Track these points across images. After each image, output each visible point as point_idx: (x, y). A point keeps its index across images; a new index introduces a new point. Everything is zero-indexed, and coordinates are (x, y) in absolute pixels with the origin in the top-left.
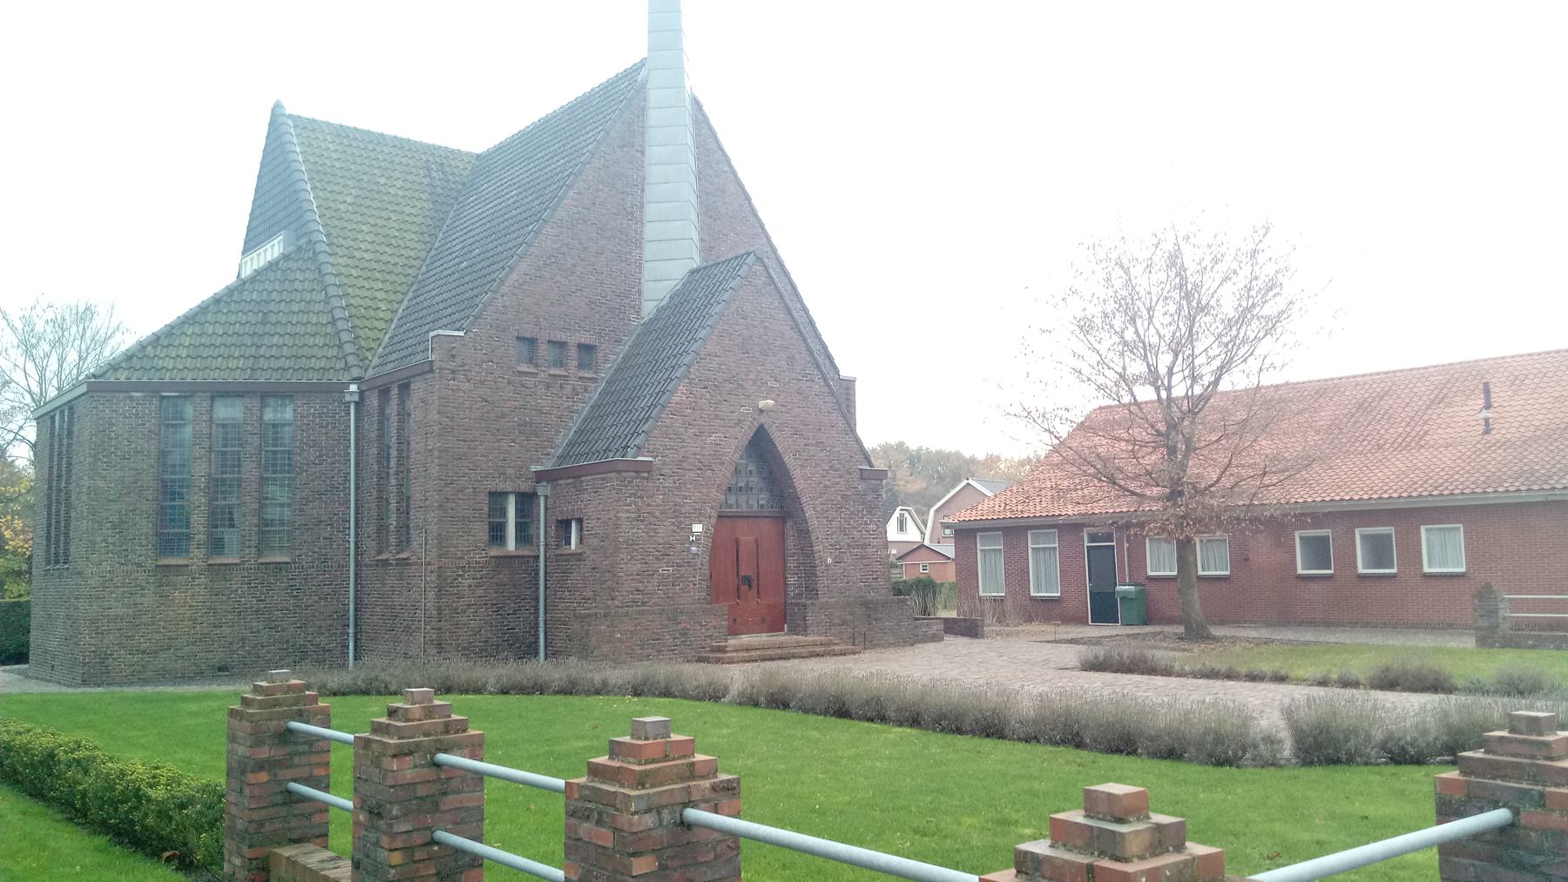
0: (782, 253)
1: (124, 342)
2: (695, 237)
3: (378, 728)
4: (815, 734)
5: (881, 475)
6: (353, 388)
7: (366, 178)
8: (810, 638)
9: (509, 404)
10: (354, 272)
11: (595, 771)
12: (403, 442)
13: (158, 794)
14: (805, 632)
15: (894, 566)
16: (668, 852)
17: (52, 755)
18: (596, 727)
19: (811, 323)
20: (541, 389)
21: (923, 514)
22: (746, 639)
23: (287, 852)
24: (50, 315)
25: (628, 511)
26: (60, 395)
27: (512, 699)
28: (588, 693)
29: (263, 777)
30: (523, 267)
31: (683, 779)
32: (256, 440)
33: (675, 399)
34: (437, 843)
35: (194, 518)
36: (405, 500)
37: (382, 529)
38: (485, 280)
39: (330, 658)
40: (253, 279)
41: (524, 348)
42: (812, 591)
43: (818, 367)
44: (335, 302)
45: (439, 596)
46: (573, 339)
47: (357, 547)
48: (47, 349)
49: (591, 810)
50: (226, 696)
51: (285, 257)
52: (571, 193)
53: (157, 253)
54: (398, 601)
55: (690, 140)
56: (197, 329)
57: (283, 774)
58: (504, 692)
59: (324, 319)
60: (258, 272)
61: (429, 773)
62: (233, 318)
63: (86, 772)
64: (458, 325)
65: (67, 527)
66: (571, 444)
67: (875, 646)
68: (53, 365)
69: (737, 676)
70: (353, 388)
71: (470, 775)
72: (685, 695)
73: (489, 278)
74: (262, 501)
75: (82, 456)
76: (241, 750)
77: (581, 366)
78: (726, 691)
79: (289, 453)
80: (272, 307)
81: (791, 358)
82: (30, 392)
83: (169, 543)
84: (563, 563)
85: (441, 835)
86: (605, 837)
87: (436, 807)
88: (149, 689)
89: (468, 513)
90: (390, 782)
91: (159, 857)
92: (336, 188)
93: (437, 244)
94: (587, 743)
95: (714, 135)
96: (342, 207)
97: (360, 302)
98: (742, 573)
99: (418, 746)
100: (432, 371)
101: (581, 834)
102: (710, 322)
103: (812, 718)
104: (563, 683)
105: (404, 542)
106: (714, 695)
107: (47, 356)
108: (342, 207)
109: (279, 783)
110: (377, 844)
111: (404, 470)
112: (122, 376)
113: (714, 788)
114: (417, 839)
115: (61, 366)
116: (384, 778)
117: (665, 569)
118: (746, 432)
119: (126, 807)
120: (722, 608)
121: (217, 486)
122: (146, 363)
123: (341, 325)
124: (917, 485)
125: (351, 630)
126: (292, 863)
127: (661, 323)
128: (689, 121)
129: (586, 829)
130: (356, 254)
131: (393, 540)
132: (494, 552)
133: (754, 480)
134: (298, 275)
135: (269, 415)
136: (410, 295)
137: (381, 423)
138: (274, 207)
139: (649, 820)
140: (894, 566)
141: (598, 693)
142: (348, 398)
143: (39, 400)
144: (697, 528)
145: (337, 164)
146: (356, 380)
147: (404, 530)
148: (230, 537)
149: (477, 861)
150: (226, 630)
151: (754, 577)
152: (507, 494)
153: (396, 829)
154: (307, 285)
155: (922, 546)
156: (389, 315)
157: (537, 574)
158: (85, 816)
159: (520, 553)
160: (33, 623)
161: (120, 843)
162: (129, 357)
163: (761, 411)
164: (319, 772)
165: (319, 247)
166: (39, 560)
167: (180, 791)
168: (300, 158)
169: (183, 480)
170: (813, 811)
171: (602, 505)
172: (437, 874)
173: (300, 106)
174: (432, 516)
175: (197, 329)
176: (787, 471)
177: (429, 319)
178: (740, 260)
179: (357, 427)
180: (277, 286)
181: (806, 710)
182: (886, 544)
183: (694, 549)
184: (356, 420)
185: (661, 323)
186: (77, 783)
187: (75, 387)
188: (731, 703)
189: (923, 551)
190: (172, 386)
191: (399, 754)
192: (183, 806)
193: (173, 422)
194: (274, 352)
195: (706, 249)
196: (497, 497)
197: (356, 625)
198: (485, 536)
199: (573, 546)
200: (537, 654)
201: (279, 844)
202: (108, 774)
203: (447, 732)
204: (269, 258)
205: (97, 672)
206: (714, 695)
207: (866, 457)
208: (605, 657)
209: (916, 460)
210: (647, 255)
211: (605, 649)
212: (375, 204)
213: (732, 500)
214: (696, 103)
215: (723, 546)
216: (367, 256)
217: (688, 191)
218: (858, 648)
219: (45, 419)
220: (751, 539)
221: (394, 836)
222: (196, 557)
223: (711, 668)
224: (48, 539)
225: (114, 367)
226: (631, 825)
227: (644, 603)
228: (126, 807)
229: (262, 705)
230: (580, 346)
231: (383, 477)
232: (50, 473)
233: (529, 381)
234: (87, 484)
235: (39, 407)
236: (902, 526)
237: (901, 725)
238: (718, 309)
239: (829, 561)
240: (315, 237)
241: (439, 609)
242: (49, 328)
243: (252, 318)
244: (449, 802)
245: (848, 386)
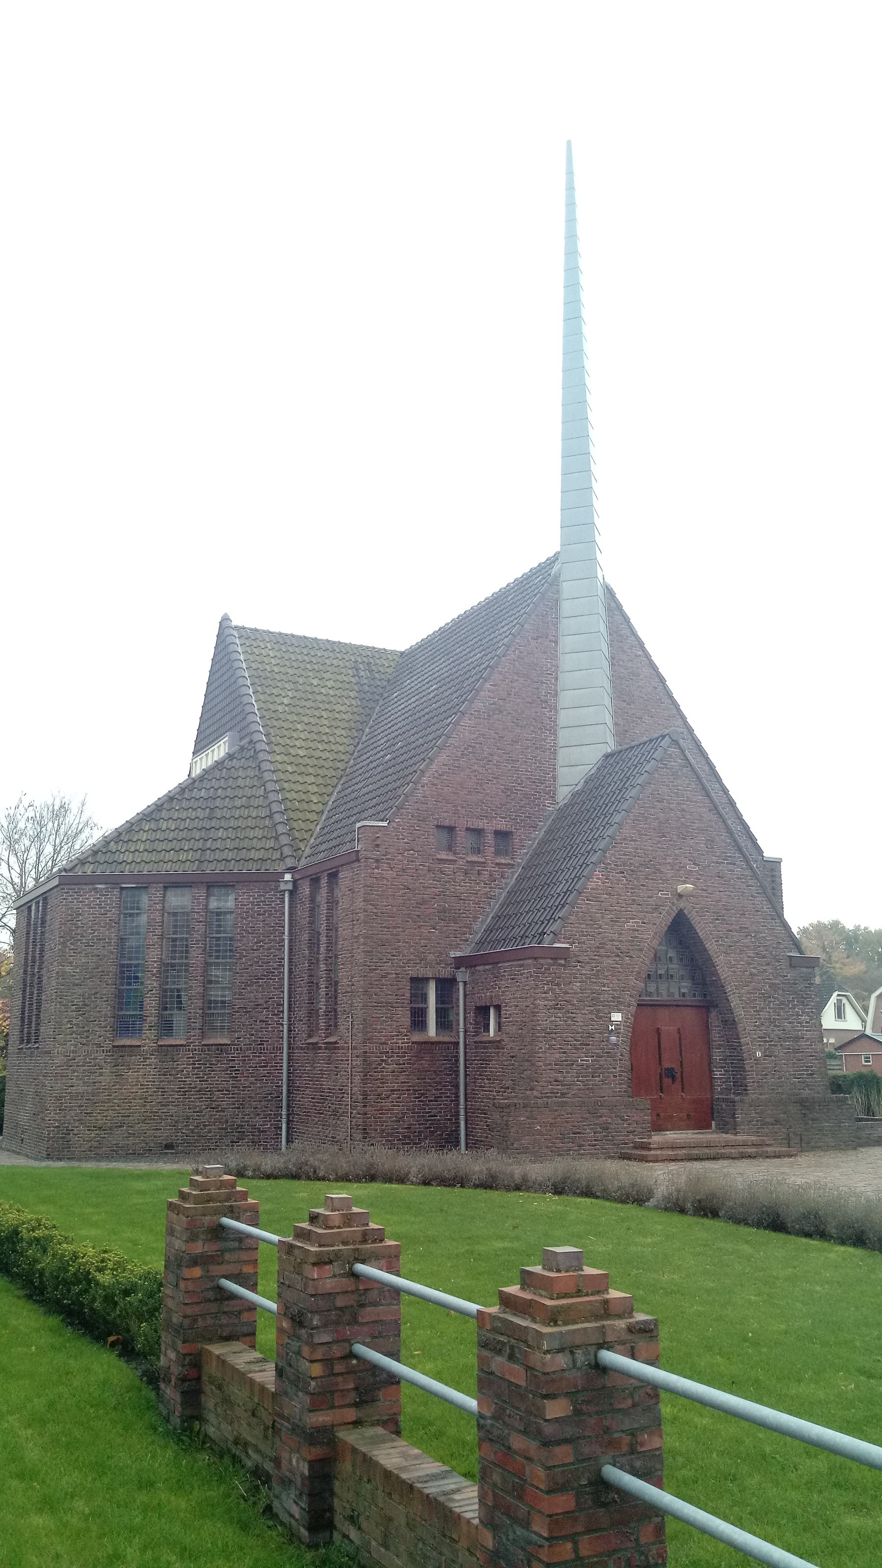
0: (700, 733)
1: (93, 837)
2: (609, 720)
3: (301, 1234)
4: (747, 1249)
5: (813, 963)
6: (288, 877)
7: (301, 681)
8: (740, 1138)
9: (429, 891)
10: (289, 768)
11: (507, 1301)
12: (332, 928)
13: (105, 1278)
14: (734, 1129)
15: (831, 1056)
16: (581, 1397)
17: (16, 1232)
18: (515, 1227)
19: (732, 803)
20: (460, 877)
21: (863, 1000)
22: (671, 1136)
23: (217, 1349)
24: (31, 813)
25: (546, 999)
26: (36, 887)
27: (435, 1190)
28: (508, 1188)
29: (197, 1272)
30: (443, 758)
31: (597, 1317)
32: (201, 927)
33: (591, 885)
34: (356, 1357)
35: (147, 1001)
36: (333, 984)
37: (312, 1013)
38: (407, 772)
39: (264, 1140)
40: (202, 778)
41: (444, 836)
42: (740, 1086)
43: (740, 850)
44: (272, 797)
45: (364, 1081)
46: (489, 826)
47: (290, 1031)
48: (27, 843)
49: (504, 1344)
50: (171, 1175)
51: (230, 757)
52: (487, 685)
53: (121, 755)
54: (326, 1084)
55: (602, 628)
56: (153, 825)
57: (215, 1270)
58: (426, 1183)
59: (263, 813)
60: (206, 772)
61: (347, 1284)
62: (184, 815)
63: (45, 1251)
64: (382, 815)
65: (38, 1009)
66: (489, 930)
67: (813, 1149)
68: (32, 860)
69: (663, 1177)
70: (288, 877)
71: (386, 1289)
72: (606, 1196)
73: (411, 770)
74: (208, 982)
75: (53, 943)
76: (178, 1244)
77: (498, 853)
78: (650, 1195)
79: (231, 939)
80: (218, 802)
81: (710, 841)
82: (12, 883)
84: (483, 1049)
85: (361, 1349)
86: (517, 1375)
87: (354, 1321)
88: (104, 1165)
89: (392, 999)
90: (311, 1291)
91: (105, 1342)
92: (275, 691)
93: (364, 738)
94: (507, 1244)
95: (627, 620)
96: (280, 708)
97: (295, 796)
98: (666, 1065)
99: (337, 1255)
100: (358, 860)
101: (493, 1367)
102: (624, 807)
103: (743, 1230)
104: (483, 1177)
105: (332, 1027)
106: (637, 1197)
107: (28, 850)
108: (280, 708)
109: (212, 1278)
110: (299, 1353)
111: (332, 957)
112: (89, 869)
113: (630, 1330)
114: (337, 1351)
115: (38, 858)
116: (306, 1285)
118: (664, 919)
119: (77, 1289)
120: (645, 1102)
121: (167, 968)
122: (109, 857)
123: (278, 818)
124: (856, 968)
125: (284, 1112)
126: (222, 1362)
127: (577, 808)
128: (601, 610)
129: (499, 1363)
130: (292, 751)
131: (322, 1024)
132: (417, 1037)
133: (674, 967)
134: (241, 773)
135: (213, 904)
136: (339, 787)
137: (312, 910)
138: (221, 711)
139: (562, 1360)
140: (831, 1056)
141: (518, 1188)
142: (283, 887)
143: (21, 891)
144: (617, 1017)
145: (276, 669)
146: (290, 869)
147: (333, 1013)
148: (179, 1019)
149: (394, 1380)
150: (173, 1110)
152: (427, 979)
153: (317, 1340)
154: (248, 782)
155: (863, 1036)
156: (319, 807)
157: (457, 1061)
158: (42, 1293)
159: (441, 1039)
160: (7, 1098)
161: (72, 1324)
162: (95, 852)
163: (680, 896)
164: (247, 1269)
165: (259, 746)
166: (14, 1038)
167: (125, 1278)
168: (244, 666)
169: (137, 966)
170: (745, 1339)
171: (518, 991)
172: (356, 1389)
174: (358, 1002)
175: (153, 825)
176: (710, 959)
177: (356, 810)
178: (657, 742)
179: (290, 914)
180: (222, 783)
181: (739, 1220)
182: (820, 1032)
184: (290, 907)
185: (577, 808)
186: (37, 1261)
187: (49, 880)
188: (657, 1207)
189: (864, 1041)
190: (132, 877)
191: (320, 1262)
192: (127, 1293)
193: (130, 912)
194: (218, 844)
195: (620, 733)
196: (418, 983)
197: (288, 1106)
198: (406, 1020)
199: (492, 1033)
200: (457, 1143)
201: (210, 1341)
202: (63, 1256)
203: (364, 1241)
204: (216, 759)
205: (60, 1147)
206: (637, 1197)
207: (796, 944)
208: (525, 1150)
209: (854, 941)
210: (561, 742)
211: (525, 1141)
212: (309, 704)
213: (652, 988)
214: (610, 593)
215: (644, 1036)
216: (301, 753)
217: (601, 677)
218: (793, 1150)
219: (24, 909)
220: (673, 1029)
221: (314, 1346)
222: (147, 1039)
223: (635, 1167)
224: (23, 1019)
225: (82, 862)
226: (544, 1364)
228: (77, 1289)
229: (197, 1200)
230: (498, 833)
231: (313, 962)
232: (26, 959)
233: (449, 868)
234: (57, 969)
235: (19, 898)
236: (840, 1014)
237: (843, 1242)
238: (633, 792)
239: (759, 1054)
240: (256, 737)
241: (365, 1095)
242: (30, 825)
243: (200, 813)
244: (368, 1314)
245: (774, 866)
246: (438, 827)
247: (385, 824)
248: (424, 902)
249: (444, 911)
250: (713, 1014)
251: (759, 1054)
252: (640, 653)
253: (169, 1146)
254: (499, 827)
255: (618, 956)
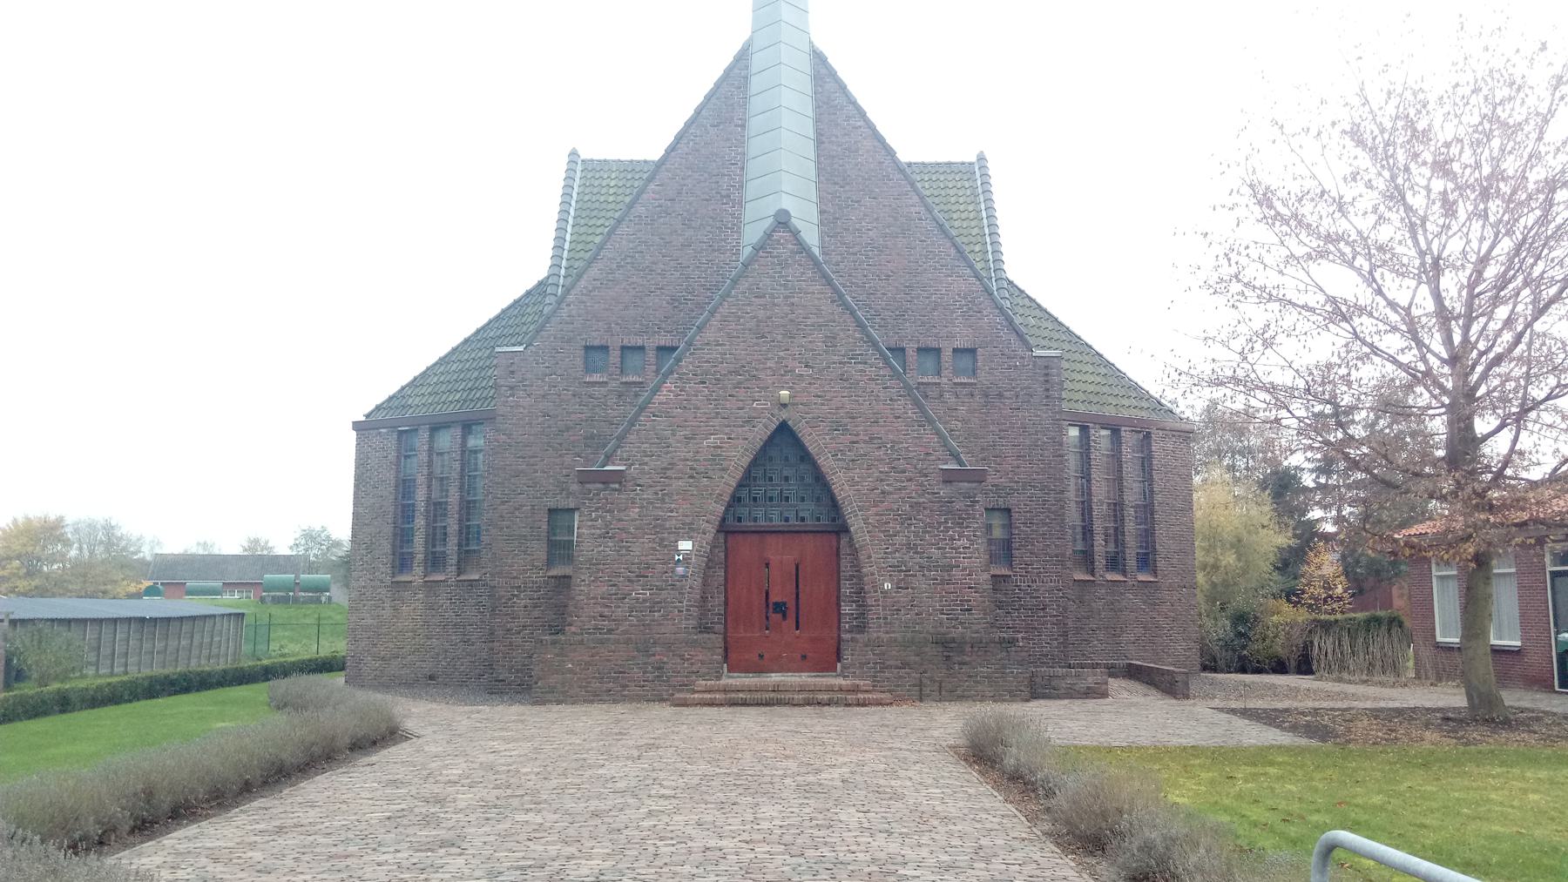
8: (840, 681)
42: (861, 628)
81: (831, 340)
83: (402, 562)
89: (524, 531)
98: (774, 598)
117: (640, 592)
144: (685, 545)
151: (791, 604)
152: (572, 511)
163: (784, 406)
173: (593, 151)
183: (680, 570)
214: (819, 58)
227: (610, 631)
230: (660, 349)
233: (597, 391)
246: (919, 350)
247: (521, 349)
248: (568, 429)
249: (592, 437)
250: (844, 541)
251: (887, 586)
252: (861, 123)
253: (431, 678)
254: (662, 343)
255: (692, 477)
